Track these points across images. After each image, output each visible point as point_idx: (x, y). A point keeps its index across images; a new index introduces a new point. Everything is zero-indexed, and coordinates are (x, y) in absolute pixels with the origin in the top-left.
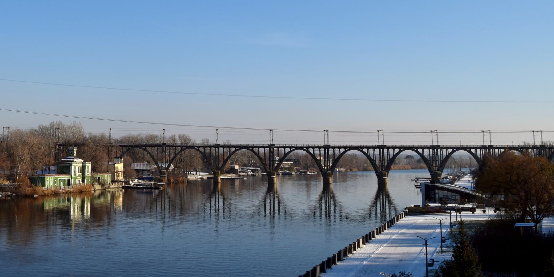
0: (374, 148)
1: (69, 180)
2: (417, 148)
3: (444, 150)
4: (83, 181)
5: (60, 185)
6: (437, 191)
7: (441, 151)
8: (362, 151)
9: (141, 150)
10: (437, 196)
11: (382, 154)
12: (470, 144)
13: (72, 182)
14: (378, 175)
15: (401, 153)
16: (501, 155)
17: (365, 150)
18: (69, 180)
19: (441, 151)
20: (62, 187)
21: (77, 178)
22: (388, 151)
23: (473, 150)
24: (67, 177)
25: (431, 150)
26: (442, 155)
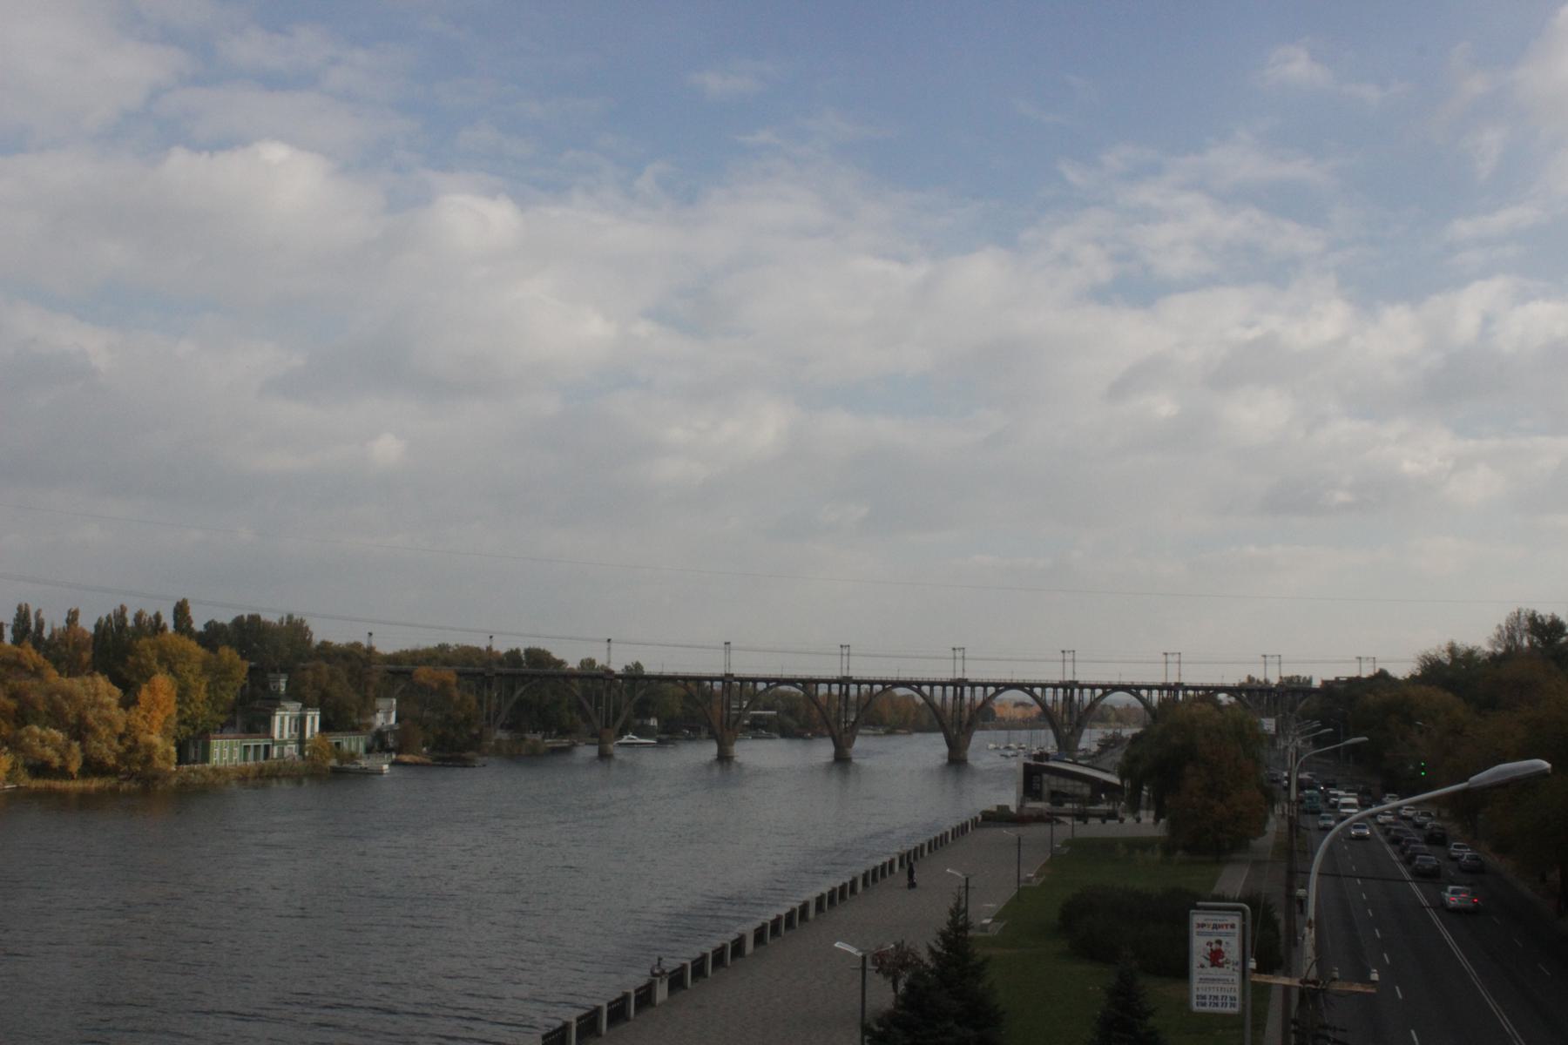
0: (944, 684)
1: (267, 747)
2: (1032, 686)
3: (1087, 691)
4: (301, 752)
5: (245, 759)
6: (1046, 776)
7: (1081, 692)
8: (1031, 693)
9: (670, 685)
10: (1046, 789)
11: (1069, 700)
12: (1138, 680)
13: (275, 752)
14: (949, 743)
15: (1000, 696)
16: (1164, 703)
17: (1038, 691)
18: (267, 747)
19: (1081, 692)
20: (251, 762)
21: (285, 743)
22: (973, 691)
23: (1038, 691)
24: (262, 742)
25: (1060, 690)
26: (972, 699)
